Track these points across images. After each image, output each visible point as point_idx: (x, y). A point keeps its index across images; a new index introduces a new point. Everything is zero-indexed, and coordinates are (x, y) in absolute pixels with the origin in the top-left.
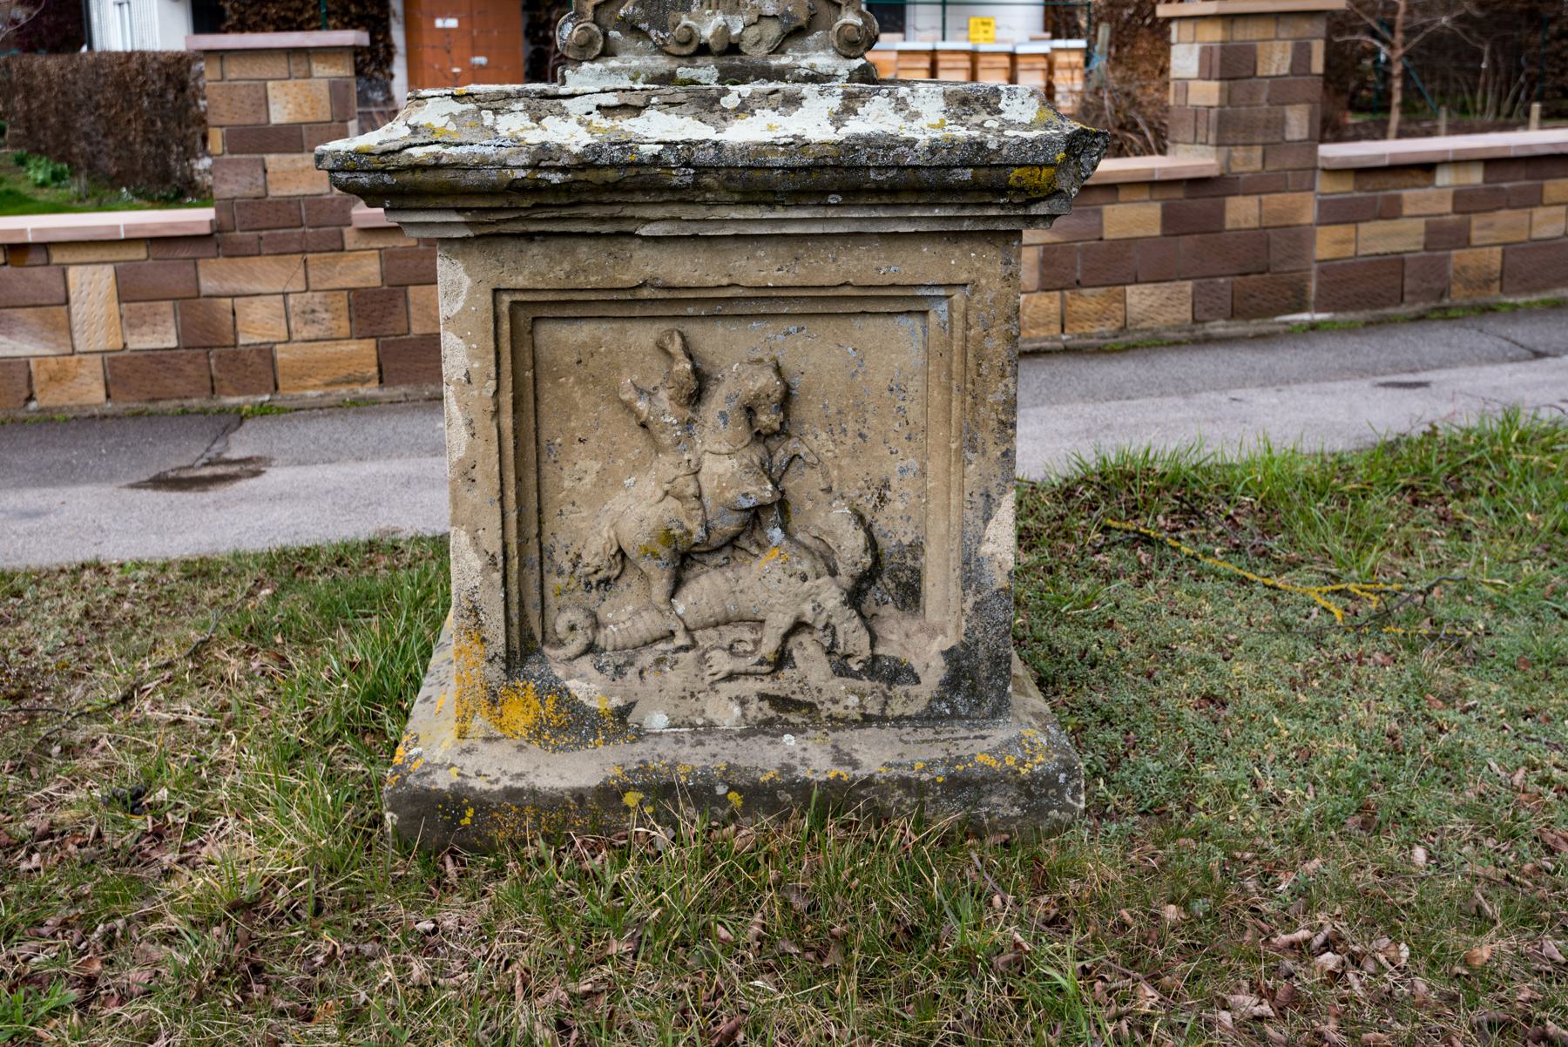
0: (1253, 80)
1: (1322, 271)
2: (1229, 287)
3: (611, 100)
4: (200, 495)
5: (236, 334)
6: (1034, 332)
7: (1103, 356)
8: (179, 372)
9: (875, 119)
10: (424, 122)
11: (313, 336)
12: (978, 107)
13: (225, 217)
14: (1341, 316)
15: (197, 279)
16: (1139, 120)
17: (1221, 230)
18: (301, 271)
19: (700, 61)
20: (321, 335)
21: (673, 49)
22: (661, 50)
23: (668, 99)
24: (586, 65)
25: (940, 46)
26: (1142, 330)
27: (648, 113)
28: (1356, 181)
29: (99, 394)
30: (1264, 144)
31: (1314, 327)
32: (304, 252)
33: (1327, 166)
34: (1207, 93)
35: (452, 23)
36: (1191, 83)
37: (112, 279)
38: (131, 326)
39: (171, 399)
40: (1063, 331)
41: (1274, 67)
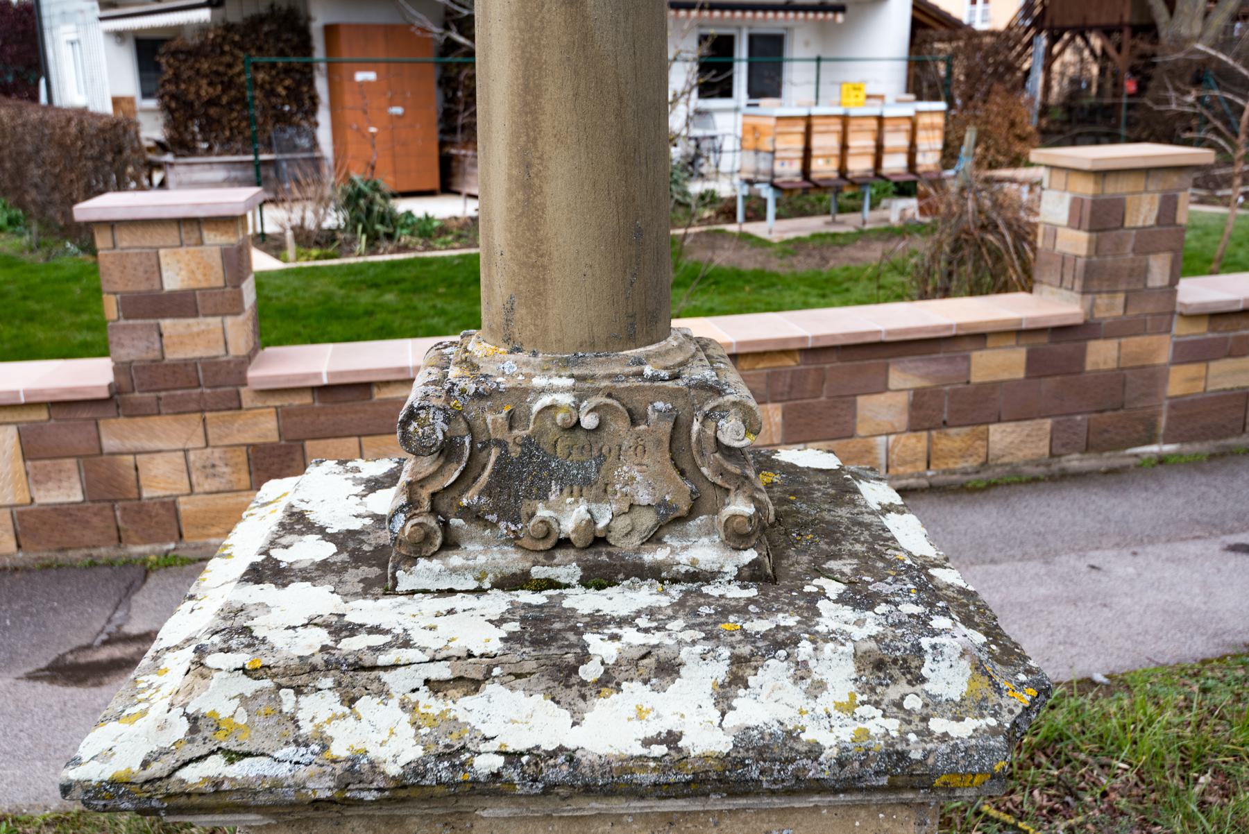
0: (1121, 231)
1: (1173, 407)
2: (1085, 424)
3: (441, 671)
4: (94, 690)
5: (139, 488)
6: (901, 469)
7: (966, 497)
8: (86, 524)
9: (770, 703)
10: (207, 710)
11: (214, 489)
12: (896, 672)
13: (124, 380)
14: (1187, 448)
15: (99, 438)
16: (1000, 222)
17: (1081, 370)
18: (200, 430)
19: (559, 556)
20: (222, 487)
21: (526, 542)
22: (514, 541)
23: (513, 669)
24: (422, 563)
25: (815, 111)
26: (1002, 465)
27: (489, 688)
28: (1210, 323)
29: (11, 546)
30: (1127, 292)
31: (1162, 460)
32: (202, 411)
33: (1185, 311)
34: (1076, 243)
35: (371, 76)
36: (1060, 231)
37: (16, 438)
38: (37, 482)
39: (79, 548)
40: (928, 467)
41: (1142, 218)
